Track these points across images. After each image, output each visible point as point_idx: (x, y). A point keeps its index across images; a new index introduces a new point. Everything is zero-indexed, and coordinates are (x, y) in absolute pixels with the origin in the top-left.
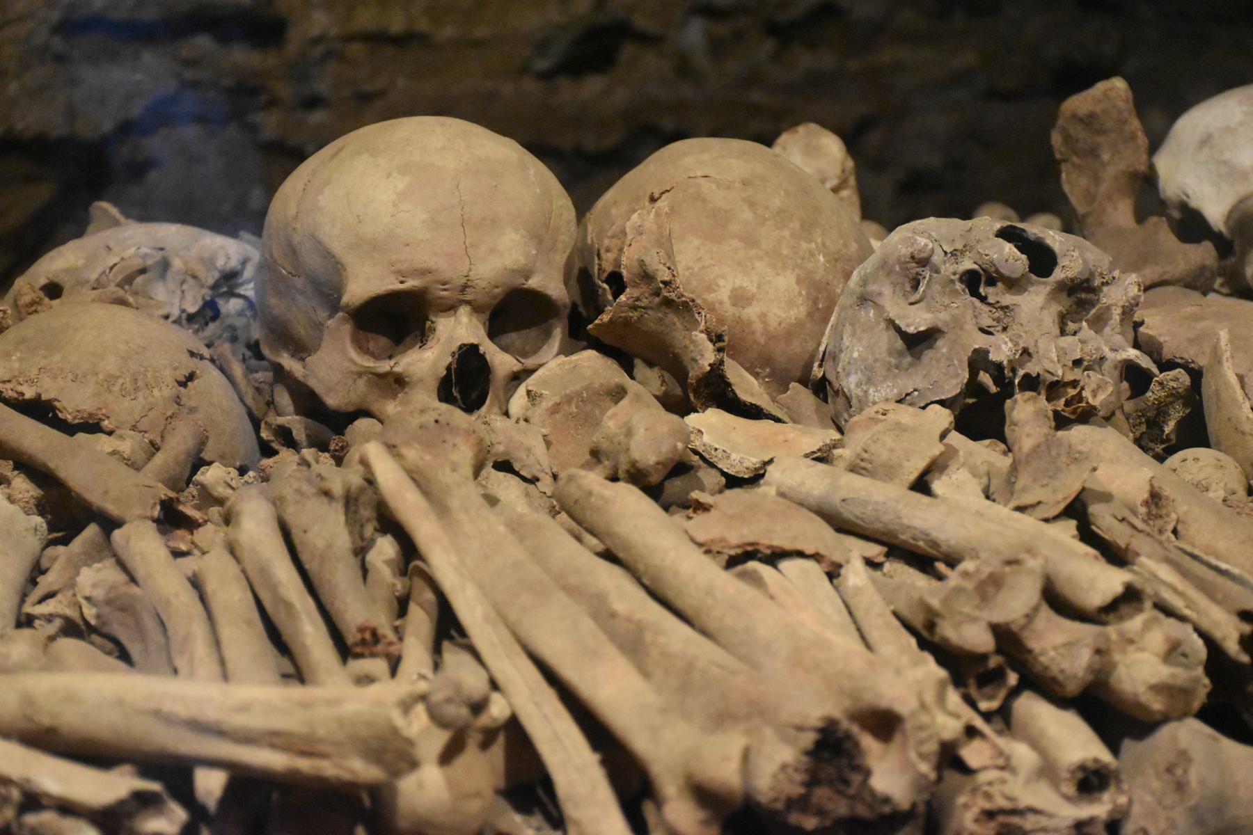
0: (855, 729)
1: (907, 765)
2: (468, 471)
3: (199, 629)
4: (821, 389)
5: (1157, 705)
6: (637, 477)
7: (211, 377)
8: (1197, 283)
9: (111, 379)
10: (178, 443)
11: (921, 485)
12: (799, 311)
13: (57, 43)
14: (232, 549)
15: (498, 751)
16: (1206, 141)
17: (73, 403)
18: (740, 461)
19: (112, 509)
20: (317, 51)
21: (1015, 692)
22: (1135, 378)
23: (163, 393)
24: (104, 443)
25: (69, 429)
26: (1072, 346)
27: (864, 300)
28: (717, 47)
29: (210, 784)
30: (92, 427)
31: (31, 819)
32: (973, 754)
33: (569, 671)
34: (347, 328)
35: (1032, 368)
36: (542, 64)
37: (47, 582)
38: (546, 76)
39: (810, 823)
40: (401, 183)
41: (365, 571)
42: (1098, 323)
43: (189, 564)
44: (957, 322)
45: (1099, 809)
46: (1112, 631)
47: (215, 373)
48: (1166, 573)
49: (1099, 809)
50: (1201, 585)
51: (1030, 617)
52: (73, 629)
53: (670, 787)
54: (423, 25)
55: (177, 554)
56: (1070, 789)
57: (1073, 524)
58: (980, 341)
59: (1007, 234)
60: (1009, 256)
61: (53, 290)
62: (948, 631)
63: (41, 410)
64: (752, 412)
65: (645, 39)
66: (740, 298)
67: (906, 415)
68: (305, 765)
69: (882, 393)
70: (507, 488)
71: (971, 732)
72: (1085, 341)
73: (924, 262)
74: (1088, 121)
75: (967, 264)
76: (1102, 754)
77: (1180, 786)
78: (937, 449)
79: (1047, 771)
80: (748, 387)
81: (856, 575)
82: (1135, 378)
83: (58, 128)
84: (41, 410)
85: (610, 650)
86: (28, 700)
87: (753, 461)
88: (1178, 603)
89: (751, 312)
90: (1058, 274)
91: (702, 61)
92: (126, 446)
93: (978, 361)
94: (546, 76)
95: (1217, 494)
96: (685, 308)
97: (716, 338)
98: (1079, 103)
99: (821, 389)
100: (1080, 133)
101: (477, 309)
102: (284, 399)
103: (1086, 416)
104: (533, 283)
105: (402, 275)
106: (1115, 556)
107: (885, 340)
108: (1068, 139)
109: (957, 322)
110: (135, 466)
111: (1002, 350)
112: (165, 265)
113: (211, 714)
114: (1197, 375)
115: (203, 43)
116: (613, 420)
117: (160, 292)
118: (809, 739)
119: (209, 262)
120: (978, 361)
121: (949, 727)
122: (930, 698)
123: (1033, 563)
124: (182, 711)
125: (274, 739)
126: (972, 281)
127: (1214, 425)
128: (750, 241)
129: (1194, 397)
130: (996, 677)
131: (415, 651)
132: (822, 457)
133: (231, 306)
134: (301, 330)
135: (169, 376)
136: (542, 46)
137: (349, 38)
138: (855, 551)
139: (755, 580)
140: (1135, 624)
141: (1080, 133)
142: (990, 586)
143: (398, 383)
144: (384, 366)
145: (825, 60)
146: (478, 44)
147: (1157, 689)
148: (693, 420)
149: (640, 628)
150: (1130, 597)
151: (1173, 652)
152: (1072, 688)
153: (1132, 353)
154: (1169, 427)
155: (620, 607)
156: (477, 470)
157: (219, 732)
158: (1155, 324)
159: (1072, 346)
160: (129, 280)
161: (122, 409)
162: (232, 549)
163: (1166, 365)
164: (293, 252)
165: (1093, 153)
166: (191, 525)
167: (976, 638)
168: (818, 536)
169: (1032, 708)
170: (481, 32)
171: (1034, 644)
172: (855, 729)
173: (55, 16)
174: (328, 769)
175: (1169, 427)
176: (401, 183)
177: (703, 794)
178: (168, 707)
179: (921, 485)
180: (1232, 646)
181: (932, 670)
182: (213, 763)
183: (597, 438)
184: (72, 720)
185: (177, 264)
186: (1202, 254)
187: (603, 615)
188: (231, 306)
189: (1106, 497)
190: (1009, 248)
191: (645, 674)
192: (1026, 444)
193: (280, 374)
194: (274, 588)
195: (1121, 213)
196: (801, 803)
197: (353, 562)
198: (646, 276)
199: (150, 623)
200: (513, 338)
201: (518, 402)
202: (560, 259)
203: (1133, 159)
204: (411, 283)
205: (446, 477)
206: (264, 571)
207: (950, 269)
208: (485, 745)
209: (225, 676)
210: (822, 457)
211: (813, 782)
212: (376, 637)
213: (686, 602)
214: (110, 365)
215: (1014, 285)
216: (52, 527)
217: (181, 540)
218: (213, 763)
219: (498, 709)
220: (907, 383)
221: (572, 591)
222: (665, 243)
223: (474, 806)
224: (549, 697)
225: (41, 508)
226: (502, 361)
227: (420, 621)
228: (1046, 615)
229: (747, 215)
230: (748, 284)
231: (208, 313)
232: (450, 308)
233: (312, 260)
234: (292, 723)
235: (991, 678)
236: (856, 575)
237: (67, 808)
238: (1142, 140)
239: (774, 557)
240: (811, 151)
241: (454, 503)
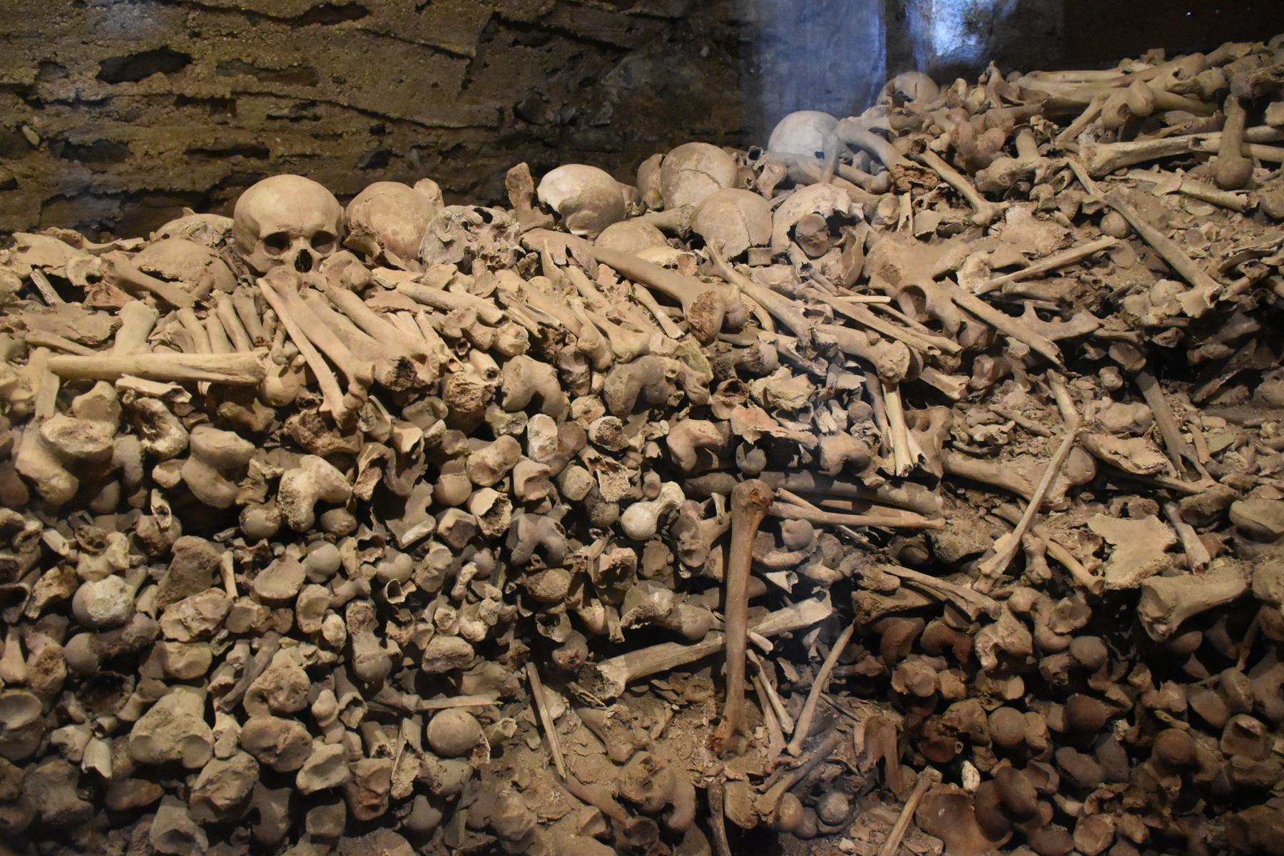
0: (413, 361)
1: (429, 370)
2: (295, 288)
3: (204, 341)
4: (421, 261)
5: (511, 351)
6: (354, 289)
7: (219, 264)
8: (547, 227)
9: (181, 264)
10: (204, 284)
11: (446, 288)
12: (415, 237)
13: (186, 157)
14: (217, 315)
15: (302, 374)
16: (552, 183)
17: (167, 273)
18: (389, 283)
19: (178, 304)
20: (281, 161)
21: (470, 349)
22: (519, 255)
23: (200, 268)
24: (178, 284)
25: (167, 281)
26: (498, 245)
27: (431, 232)
28: (422, 159)
29: (204, 387)
30: (175, 279)
31: (140, 400)
32: (453, 367)
33: (323, 347)
34: (263, 245)
35: (485, 252)
36: (360, 165)
37: (156, 330)
38: (362, 169)
39: (398, 389)
40: (277, 197)
41: (262, 320)
42: (507, 238)
43: (203, 322)
44: (460, 238)
45: (495, 383)
46: (499, 330)
47: (221, 262)
48: (517, 312)
49: (495, 383)
50: (528, 315)
51: (472, 326)
52: (163, 343)
53: (351, 380)
54: (318, 151)
55: (200, 319)
56: (485, 377)
57: (492, 299)
58: (468, 244)
59: (476, 210)
60: (477, 218)
61: (166, 236)
62: (448, 331)
63: (157, 275)
64: (395, 268)
65: (396, 156)
66: (395, 233)
67: (443, 267)
68: (230, 378)
69: (437, 261)
70: (313, 294)
71: (452, 361)
72: (502, 243)
73: (449, 219)
74: (515, 177)
75: (463, 220)
76: (495, 366)
77: (518, 375)
78: (451, 277)
79: (477, 371)
80: (393, 259)
81: (421, 316)
82: (519, 255)
83: (189, 188)
84: (157, 275)
85: (337, 340)
86: (137, 362)
87: (394, 283)
88: (520, 321)
89: (399, 237)
90: (493, 223)
91: (417, 164)
92: (187, 285)
93: (468, 251)
94: (362, 169)
95: (543, 290)
96: (372, 235)
97: (382, 245)
98: (512, 171)
99: (421, 261)
100: (513, 180)
101: (306, 238)
102: (246, 270)
103: (503, 267)
104: (325, 229)
105: (279, 227)
106: (501, 306)
107: (438, 244)
108: (510, 183)
109: (460, 238)
110: (189, 292)
111: (474, 247)
112: (205, 228)
113: (198, 363)
114: (539, 254)
115: (240, 157)
116: (346, 271)
117: (205, 236)
118: (396, 363)
119: (221, 226)
120: (468, 251)
121: (443, 359)
122: (437, 350)
123: (474, 309)
124: (190, 364)
125: (219, 370)
126: (465, 225)
127: (545, 269)
128: (397, 214)
129: (539, 260)
130: (463, 345)
131: (277, 344)
132: (417, 281)
133: (230, 241)
134: (249, 247)
135: (202, 263)
136: (361, 158)
137: (292, 156)
138: (422, 309)
139: (388, 319)
140: (505, 326)
141: (513, 180)
142: (461, 317)
143: (282, 262)
144: (276, 257)
145: (460, 163)
146: (338, 158)
147: (512, 346)
148: (374, 271)
149: (348, 333)
150: (504, 319)
151: (518, 335)
152: (486, 347)
153: (517, 247)
154: (532, 270)
155: (342, 327)
156: (299, 289)
157: (202, 370)
158: (527, 238)
159: (498, 245)
160: (193, 232)
161: (185, 273)
162: (217, 315)
163: (528, 251)
164: (243, 221)
165: (517, 187)
166: (206, 309)
167: (456, 333)
168: (411, 304)
169: (476, 354)
170: (339, 154)
171: (474, 334)
172: (413, 361)
173: (184, 148)
174: (237, 379)
175: (532, 270)
176: (277, 197)
177: (360, 381)
178: (184, 362)
179: (446, 288)
180: (536, 333)
181: (442, 341)
182: (207, 380)
183: (342, 277)
184: (153, 369)
185: (210, 227)
186: (550, 218)
187: (337, 331)
188: (230, 241)
189: (504, 291)
190: (477, 214)
191: (349, 347)
192: (478, 274)
193: (245, 263)
194: (229, 325)
195: (527, 206)
196: (395, 383)
197: (258, 318)
198: (360, 226)
199: (188, 340)
200: (321, 247)
201: (321, 268)
202: (334, 221)
203: (531, 189)
204: (283, 230)
205: (287, 289)
206: (227, 321)
207: (458, 221)
208: (297, 372)
209: (212, 351)
210: (417, 281)
211: (398, 376)
212: (263, 340)
213: (363, 325)
214: (181, 259)
215: (478, 226)
216: (161, 313)
217: (203, 314)
218: (207, 380)
219: (300, 360)
220: (444, 258)
221: (327, 323)
222: (368, 216)
223: (292, 389)
224: (319, 356)
225: (157, 306)
226: (316, 255)
227: (279, 336)
228: (478, 326)
229: (396, 206)
230: (397, 228)
231: (223, 242)
232: (297, 238)
233: (250, 224)
234: (225, 365)
235: (462, 345)
236: (421, 316)
237: (151, 396)
238: (532, 183)
239: (395, 311)
240: (427, 187)
241: (289, 297)
